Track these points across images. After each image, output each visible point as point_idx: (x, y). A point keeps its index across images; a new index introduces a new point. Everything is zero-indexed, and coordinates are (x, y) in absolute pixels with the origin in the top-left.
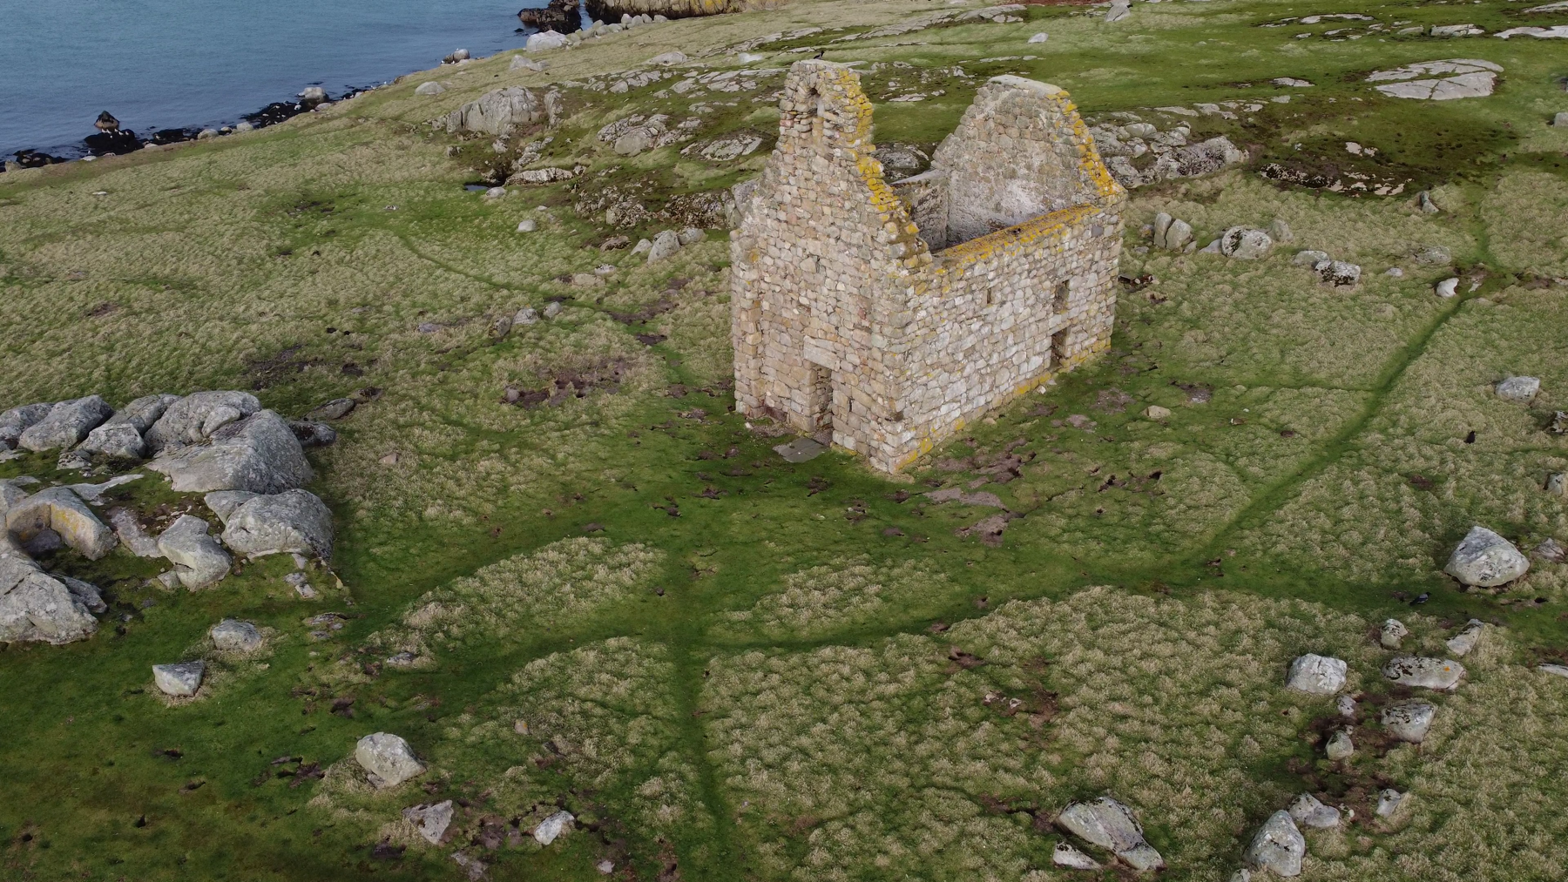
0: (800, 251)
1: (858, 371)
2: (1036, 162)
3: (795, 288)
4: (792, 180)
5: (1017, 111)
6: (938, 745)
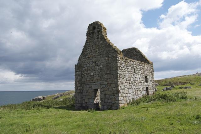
0: (91, 63)
4: (89, 48)
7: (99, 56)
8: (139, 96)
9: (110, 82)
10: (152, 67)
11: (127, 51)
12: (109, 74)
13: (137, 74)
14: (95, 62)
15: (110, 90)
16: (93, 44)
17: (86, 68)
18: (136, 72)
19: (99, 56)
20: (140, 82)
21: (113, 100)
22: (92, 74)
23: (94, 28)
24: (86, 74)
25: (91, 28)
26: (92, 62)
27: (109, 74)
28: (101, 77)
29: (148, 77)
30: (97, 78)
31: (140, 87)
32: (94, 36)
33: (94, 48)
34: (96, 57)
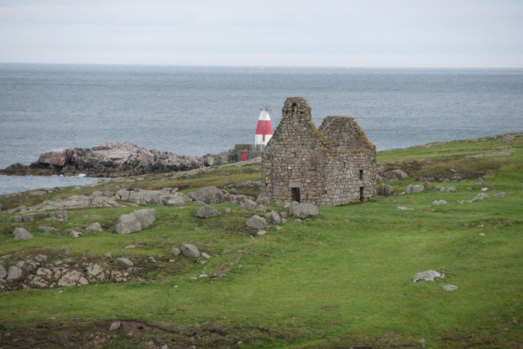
0: (288, 152)
1: (310, 185)
2: (346, 140)
3: (286, 164)
4: (286, 131)
5: (338, 124)
6: (53, 332)
7: (301, 146)
8: (349, 198)
9: (315, 180)
10: (373, 154)
11: (334, 122)
12: (313, 170)
13: (347, 169)
14: (295, 153)
15: (314, 189)
16: (291, 128)
17: (280, 158)
18: (346, 167)
19: (301, 146)
20: (351, 179)
21: (319, 201)
22: (289, 168)
23: (294, 105)
25: (290, 105)
27: (313, 170)
28: (302, 173)
29: (364, 172)
30: (297, 174)
31: (351, 186)
32: (294, 116)
33: (293, 134)
34: (296, 145)
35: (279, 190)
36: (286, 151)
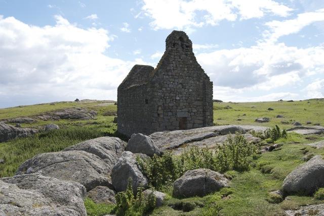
0: (176, 83)
7: (187, 78)
19: (187, 78)
24: (168, 97)
26: (178, 83)
28: (189, 103)
30: (185, 104)
35: (168, 121)
36: (174, 82)
